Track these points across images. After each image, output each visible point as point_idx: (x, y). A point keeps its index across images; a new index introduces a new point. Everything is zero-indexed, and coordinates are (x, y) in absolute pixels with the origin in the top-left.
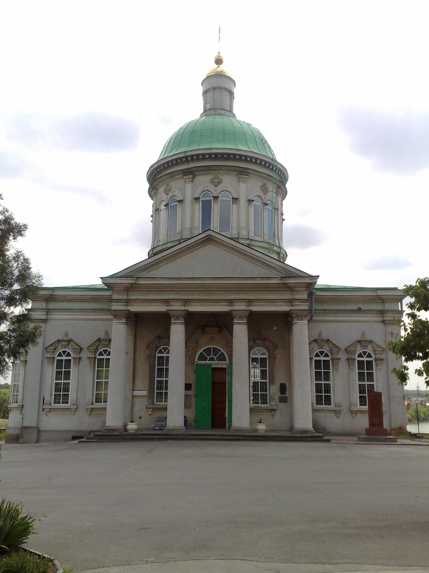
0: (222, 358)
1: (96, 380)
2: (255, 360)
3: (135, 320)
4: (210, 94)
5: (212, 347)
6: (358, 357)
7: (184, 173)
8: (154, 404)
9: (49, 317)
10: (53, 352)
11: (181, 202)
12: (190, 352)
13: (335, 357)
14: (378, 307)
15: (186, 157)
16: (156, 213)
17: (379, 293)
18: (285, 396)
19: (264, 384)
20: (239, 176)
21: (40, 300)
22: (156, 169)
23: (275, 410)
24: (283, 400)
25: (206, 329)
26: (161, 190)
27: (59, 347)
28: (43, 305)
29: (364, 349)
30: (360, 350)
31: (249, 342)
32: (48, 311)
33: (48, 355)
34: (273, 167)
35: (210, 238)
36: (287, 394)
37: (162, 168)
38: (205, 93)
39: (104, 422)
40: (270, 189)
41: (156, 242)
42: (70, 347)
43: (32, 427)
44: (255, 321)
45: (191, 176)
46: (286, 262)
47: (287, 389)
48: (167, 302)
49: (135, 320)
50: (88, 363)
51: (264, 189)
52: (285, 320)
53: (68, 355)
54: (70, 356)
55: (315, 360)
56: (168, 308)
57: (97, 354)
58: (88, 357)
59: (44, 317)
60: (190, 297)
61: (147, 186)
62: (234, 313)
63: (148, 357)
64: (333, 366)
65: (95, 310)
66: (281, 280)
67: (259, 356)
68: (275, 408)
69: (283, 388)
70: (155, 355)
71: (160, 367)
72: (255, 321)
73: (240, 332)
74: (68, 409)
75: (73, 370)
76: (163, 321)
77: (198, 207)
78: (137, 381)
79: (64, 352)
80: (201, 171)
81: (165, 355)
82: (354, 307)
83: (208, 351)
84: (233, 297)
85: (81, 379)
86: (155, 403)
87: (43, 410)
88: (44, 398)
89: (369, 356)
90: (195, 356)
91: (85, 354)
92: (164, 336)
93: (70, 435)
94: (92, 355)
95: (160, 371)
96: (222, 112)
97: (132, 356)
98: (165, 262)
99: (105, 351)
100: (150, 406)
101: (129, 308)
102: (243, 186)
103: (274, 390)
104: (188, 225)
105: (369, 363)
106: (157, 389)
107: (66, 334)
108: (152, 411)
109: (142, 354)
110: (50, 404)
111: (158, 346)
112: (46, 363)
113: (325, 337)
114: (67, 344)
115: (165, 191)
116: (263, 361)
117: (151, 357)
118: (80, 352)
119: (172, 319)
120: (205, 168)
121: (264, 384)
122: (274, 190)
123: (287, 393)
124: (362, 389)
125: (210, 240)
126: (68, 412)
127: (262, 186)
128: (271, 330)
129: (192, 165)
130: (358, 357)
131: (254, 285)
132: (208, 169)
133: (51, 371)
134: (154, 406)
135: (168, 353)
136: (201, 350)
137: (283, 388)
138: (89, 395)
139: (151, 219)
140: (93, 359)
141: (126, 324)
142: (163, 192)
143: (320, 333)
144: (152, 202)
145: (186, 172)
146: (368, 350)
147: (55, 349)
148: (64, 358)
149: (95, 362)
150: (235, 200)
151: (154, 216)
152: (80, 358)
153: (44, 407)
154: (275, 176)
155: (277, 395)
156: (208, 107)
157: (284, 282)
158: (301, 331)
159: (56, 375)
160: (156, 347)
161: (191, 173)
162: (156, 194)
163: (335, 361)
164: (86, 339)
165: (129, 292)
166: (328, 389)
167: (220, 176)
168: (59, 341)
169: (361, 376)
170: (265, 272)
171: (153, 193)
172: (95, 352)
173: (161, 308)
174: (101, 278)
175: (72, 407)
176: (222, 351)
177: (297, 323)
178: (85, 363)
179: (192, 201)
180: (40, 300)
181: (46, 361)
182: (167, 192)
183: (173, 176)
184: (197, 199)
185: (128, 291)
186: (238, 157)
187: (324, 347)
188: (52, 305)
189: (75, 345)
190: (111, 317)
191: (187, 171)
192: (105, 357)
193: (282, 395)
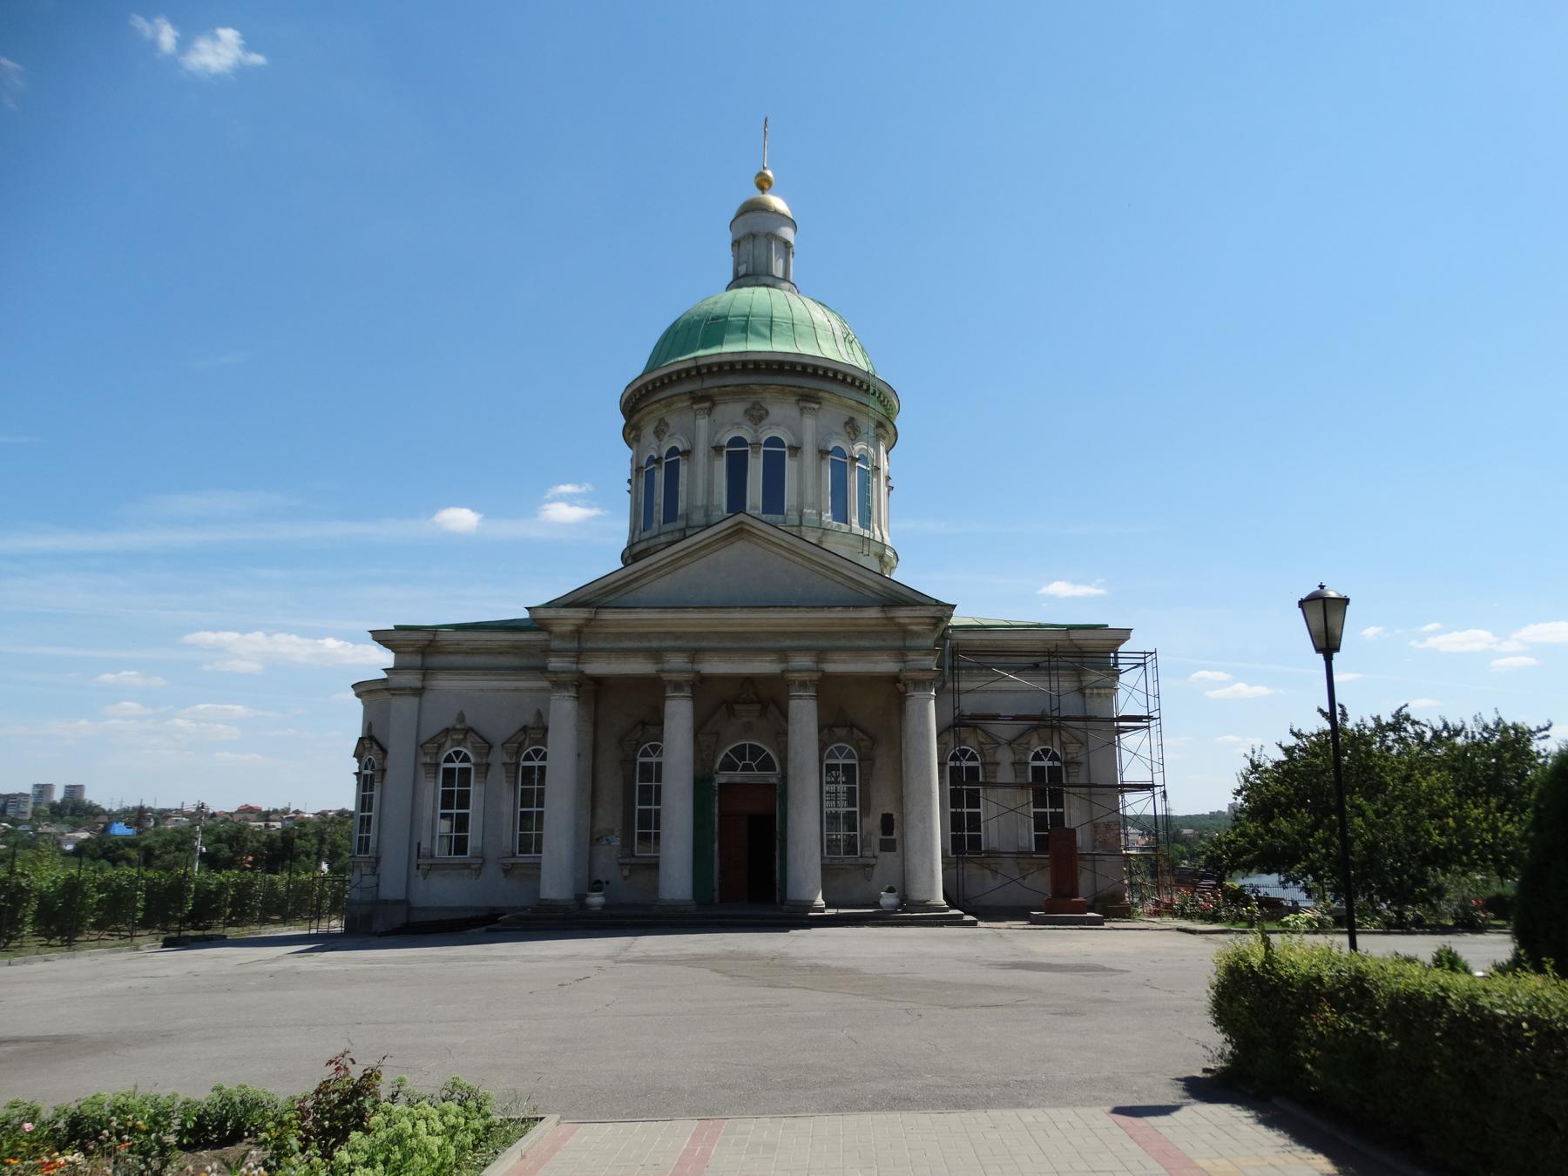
0: (767, 764)
2: (831, 768)
3: (593, 691)
4: (747, 247)
9: (427, 684)
13: (988, 759)
17: (1075, 635)
19: (850, 817)
20: (802, 404)
22: (639, 390)
23: (868, 865)
27: (448, 743)
31: (820, 731)
32: (426, 671)
36: (895, 835)
38: (736, 244)
39: (538, 891)
40: (863, 429)
43: (398, 902)
44: (827, 688)
45: (707, 405)
46: (350, 805)
48: (656, 654)
49: (593, 691)
53: (466, 759)
59: (418, 684)
61: (621, 421)
65: (516, 670)
67: (841, 761)
68: (873, 861)
69: (887, 823)
73: (804, 715)
74: (467, 866)
75: (475, 789)
76: (652, 691)
77: (721, 465)
79: (457, 753)
80: (727, 394)
81: (654, 759)
83: (739, 752)
85: (494, 804)
89: (1054, 757)
90: (714, 761)
91: (498, 757)
92: (654, 722)
95: (645, 791)
96: (770, 281)
99: (537, 752)
101: (581, 667)
102: (809, 422)
104: (700, 500)
105: (465, 772)
107: (461, 718)
110: (514, 855)
116: (849, 770)
121: (850, 817)
127: (846, 423)
128: (863, 724)
129: (708, 383)
132: (741, 392)
133: (432, 790)
134: (633, 861)
135: (544, 758)
136: (727, 750)
137: (887, 823)
138: (508, 835)
139: (628, 487)
141: (577, 698)
144: (629, 453)
145: (696, 398)
147: (439, 748)
148: (457, 765)
149: (436, 773)
150: (796, 450)
152: (488, 765)
155: (877, 836)
156: (742, 270)
158: (928, 714)
161: (705, 401)
162: (637, 439)
163: (989, 768)
164: (500, 727)
168: (447, 731)
173: (885, 665)
176: (768, 750)
178: (498, 774)
181: (422, 771)
182: (659, 433)
184: (718, 449)
190: (546, 684)
192: (536, 763)
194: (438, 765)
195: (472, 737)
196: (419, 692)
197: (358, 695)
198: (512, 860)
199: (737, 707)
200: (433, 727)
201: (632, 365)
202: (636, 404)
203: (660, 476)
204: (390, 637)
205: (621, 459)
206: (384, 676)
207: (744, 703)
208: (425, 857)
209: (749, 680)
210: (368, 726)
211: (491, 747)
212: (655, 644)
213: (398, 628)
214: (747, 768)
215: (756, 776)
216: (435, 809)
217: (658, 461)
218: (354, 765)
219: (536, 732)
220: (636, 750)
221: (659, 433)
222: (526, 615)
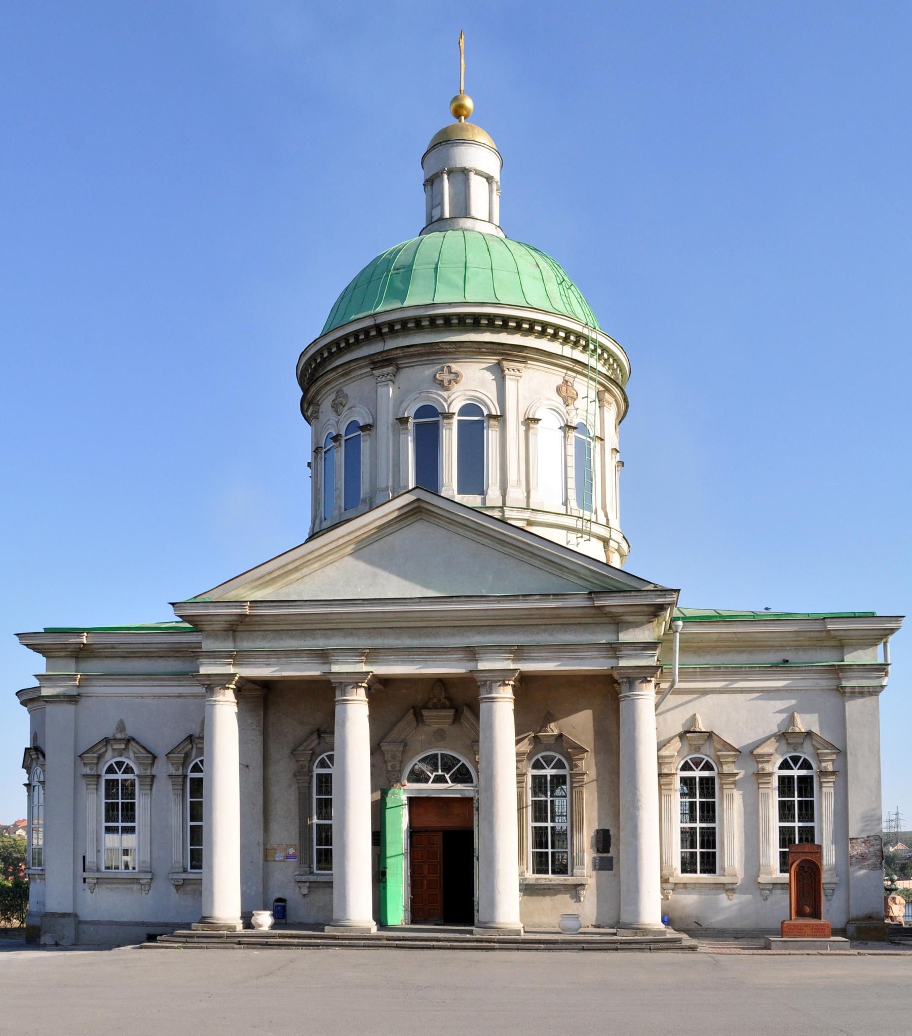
0: (463, 776)
1: (190, 824)
5: (439, 752)
6: (191, 772)
7: (373, 363)
8: (312, 873)
9: (82, 690)
10: (97, 764)
11: (369, 430)
12: (389, 764)
14: (828, 658)
15: (378, 327)
16: (316, 458)
18: (609, 855)
21: (63, 654)
22: (313, 358)
24: (605, 864)
25: (425, 713)
26: (326, 405)
28: (68, 667)
29: (795, 751)
30: (110, 759)
33: (87, 771)
34: (587, 341)
35: (419, 507)
37: (326, 355)
40: (582, 391)
41: (318, 522)
42: (131, 755)
43: (64, 915)
45: (390, 369)
47: (613, 840)
48: (324, 655)
49: (259, 697)
50: (171, 787)
51: (566, 394)
52: (607, 693)
53: (128, 770)
54: (133, 772)
55: (106, 780)
56: (325, 668)
57: (187, 768)
58: (170, 776)
60: (378, 642)
62: (480, 677)
63: (295, 775)
64: (722, 789)
66: (591, 599)
70: (311, 771)
71: (323, 794)
72: (538, 699)
75: (140, 801)
78: (274, 827)
80: (412, 356)
82: (775, 657)
84: (475, 640)
86: (315, 871)
87: (84, 882)
88: (84, 857)
89: (806, 765)
91: (163, 769)
92: (324, 732)
93: (143, 932)
94: (177, 770)
97: (259, 774)
98: (316, 565)
100: (303, 878)
103: (584, 844)
106: (319, 844)
107: (121, 727)
108: (309, 887)
109: (283, 770)
110: (185, 871)
111: (318, 750)
112: (84, 787)
113: (701, 726)
114: (123, 746)
115: (333, 407)
117: (302, 773)
118: (152, 764)
119: (338, 693)
120: (422, 350)
122: (593, 395)
123: (612, 849)
124: (786, 837)
125: (420, 511)
126: (136, 887)
130: (191, 772)
131: (482, 613)
134: (312, 878)
137: (603, 841)
140: (181, 779)
142: (330, 408)
143: (693, 718)
144: (306, 430)
146: (804, 753)
147: (100, 758)
148: (120, 776)
149: (184, 784)
150: (500, 418)
151: (313, 465)
152: (153, 777)
153: (86, 875)
154: (593, 362)
157: (597, 603)
158: (650, 719)
159: (107, 810)
160: (313, 754)
164: (163, 737)
165: (237, 634)
166: (709, 838)
167: (455, 367)
168: (107, 741)
169: (785, 811)
170: (550, 583)
171: (309, 413)
172: (184, 764)
173: (312, 670)
174: (173, 604)
175: (142, 876)
177: (627, 696)
178: (163, 785)
179: (393, 425)
180: (63, 654)
181: (83, 783)
182: (337, 407)
183: (350, 372)
184: (403, 421)
185: (234, 631)
186: (499, 323)
187: (703, 749)
188: (94, 666)
189: (141, 750)
191: (380, 358)
193: (698, 780)
194: (99, 776)
195: (133, 746)
196: (72, 699)
197: (24, 703)
198: (184, 876)
199: (425, 713)
200: (92, 737)
201: (309, 327)
202: (317, 372)
203: (340, 455)
204: (191, 618)
205: (300, 436)
206: (36, 683)
207: (435, 707)
208: (92, 870)
209: (441, 681)
210: (34, 737)
211: (154, 757)
212: (321, 643)
213: (48, 631)
214: (440, 779)
215: (451, 789)
216: (98, 822)
217: (336, 438)
218: (23, 776)
219: (194, 747)
220: (312, 761)
221: (337, 407)
222: (170, 618)
